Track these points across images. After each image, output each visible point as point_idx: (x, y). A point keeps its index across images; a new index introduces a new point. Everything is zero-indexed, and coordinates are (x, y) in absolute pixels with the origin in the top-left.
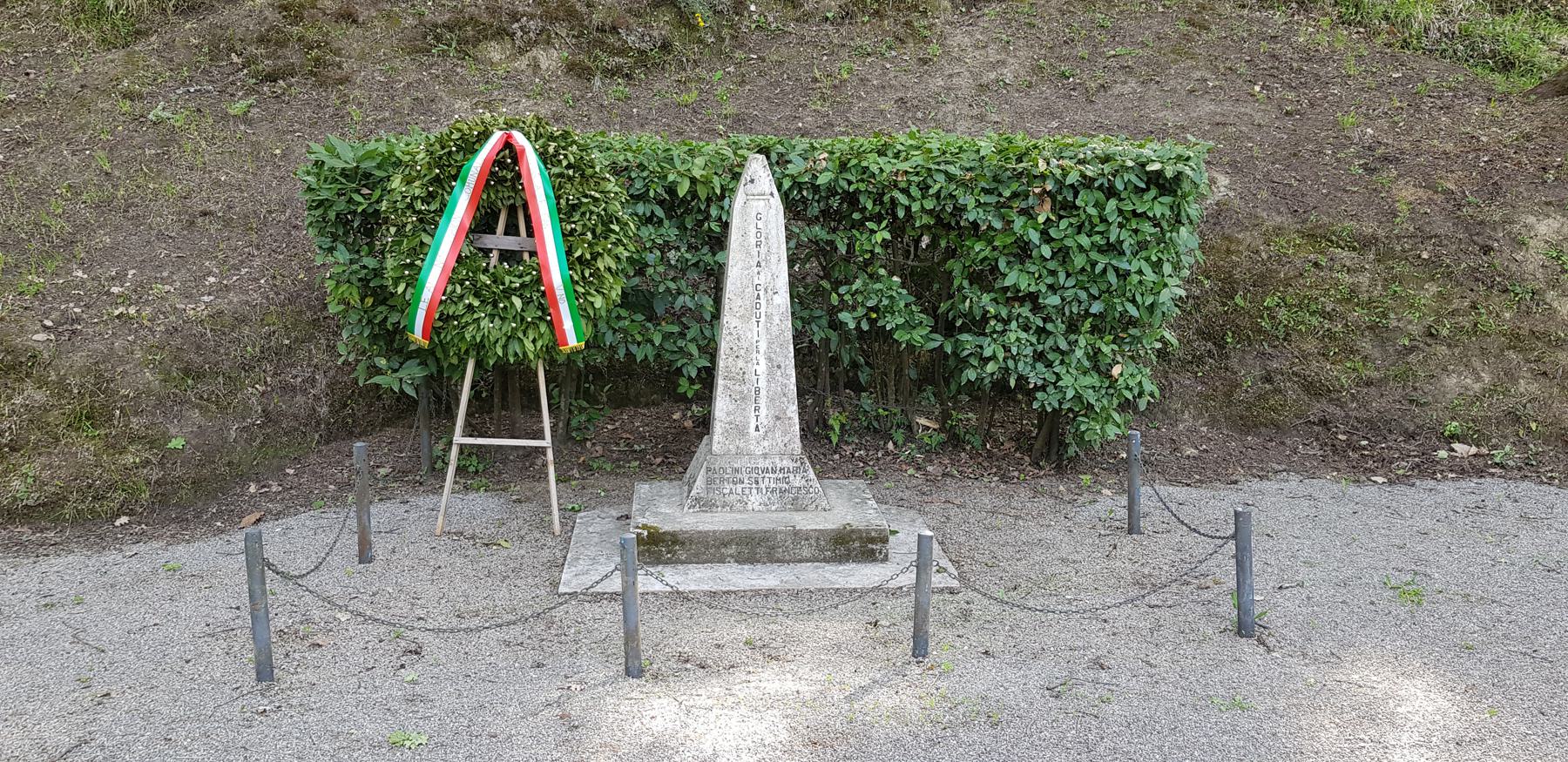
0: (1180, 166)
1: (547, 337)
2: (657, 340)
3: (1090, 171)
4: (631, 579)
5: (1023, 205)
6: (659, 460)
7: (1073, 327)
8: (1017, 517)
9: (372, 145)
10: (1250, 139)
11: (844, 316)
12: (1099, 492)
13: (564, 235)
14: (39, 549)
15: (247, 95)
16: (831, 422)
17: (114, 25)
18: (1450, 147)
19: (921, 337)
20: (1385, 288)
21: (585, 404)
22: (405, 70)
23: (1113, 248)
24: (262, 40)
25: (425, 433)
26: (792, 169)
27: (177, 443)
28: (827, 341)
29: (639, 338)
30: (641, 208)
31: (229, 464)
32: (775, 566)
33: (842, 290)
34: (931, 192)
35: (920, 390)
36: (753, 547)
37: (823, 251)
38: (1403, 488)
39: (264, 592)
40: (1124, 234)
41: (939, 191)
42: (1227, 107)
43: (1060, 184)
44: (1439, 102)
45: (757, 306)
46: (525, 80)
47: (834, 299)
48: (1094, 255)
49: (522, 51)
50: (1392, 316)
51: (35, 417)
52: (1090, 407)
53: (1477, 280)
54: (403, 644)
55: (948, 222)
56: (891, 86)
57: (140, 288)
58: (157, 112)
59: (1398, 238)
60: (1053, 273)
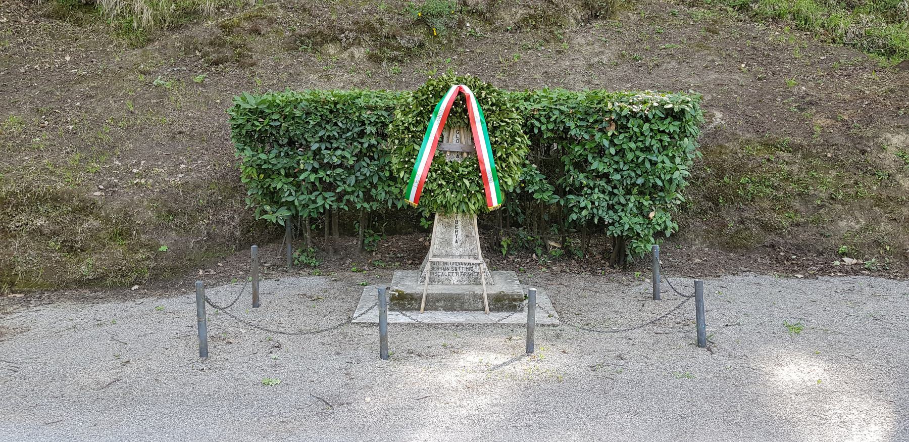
0: (683, 106)
3: (636, 109)
5: (600, 127)
7: (628, 192)
8: (596, 292)
9: (265, 96)
10: (736, 93)
12: (644, 281)
14: (95, 300)
15: (203, 72)
16: (502, 243)
17: (136, 36)
18: (847, 97)
19: (548, 196)
20: (807, 173)
21: (372, 232)
22: (285, 59)
23: (648, 149)
24: (211, 44)
25: (289, 246)
27: (163, 248)
31: (190, 260)
34: (552, 120)
36: (453, 303)
38: (812, 280)
39: (205, 313)
40: (654, 142)
42: (725, 75)
43: (619, 115)
44: (845, 73)
48: (638, 153)
49: (345, 49)
50: (811, 188)
51: (94, 234)
52: (638, 234)
53: (858, 168)
54: (272, 343)
55: (563, 135)
57: (147, 170)
58: (158, 81)
59: (815, 146)
60: (617, 163)
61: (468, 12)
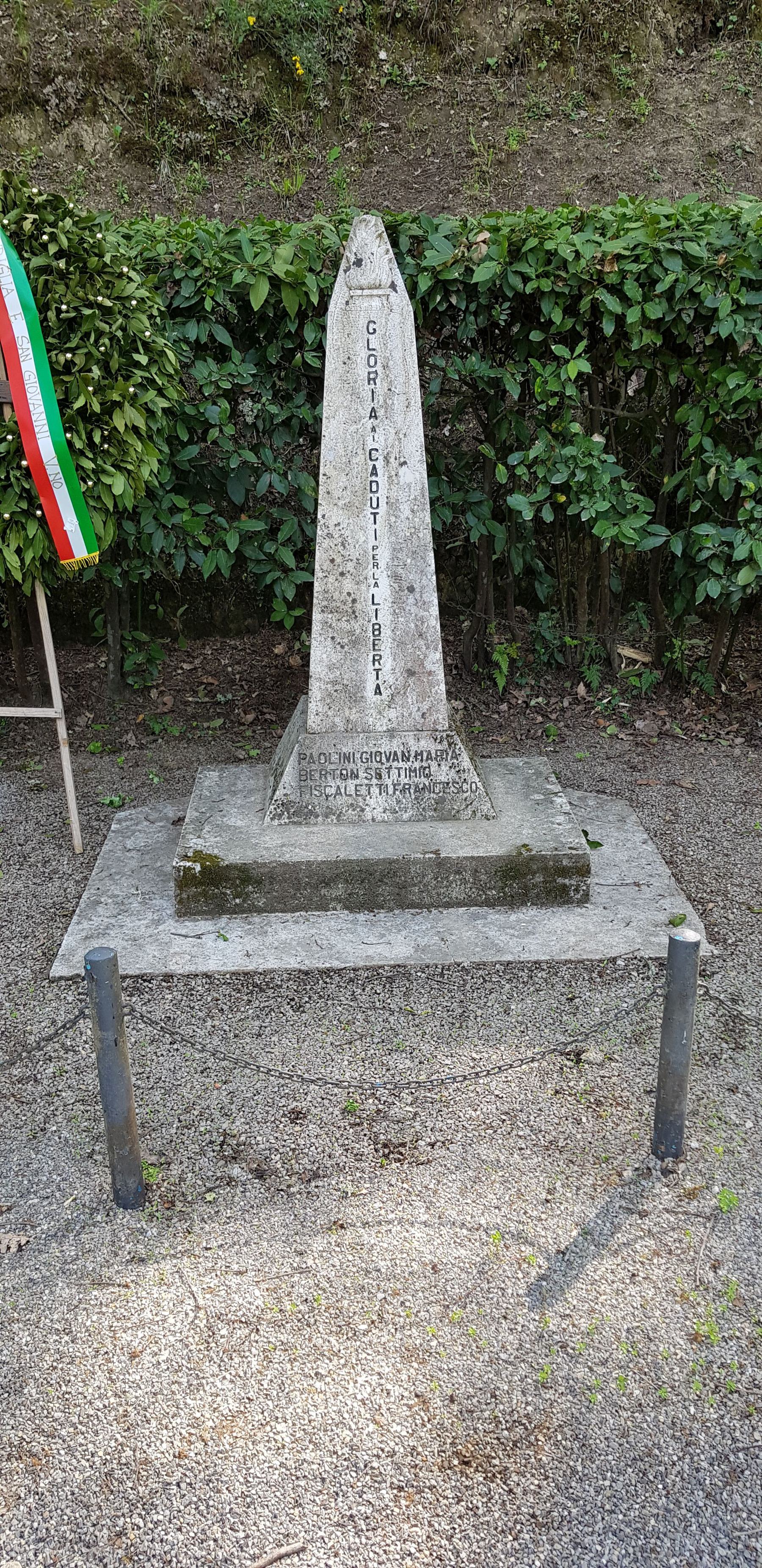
1: (41, 544)
2: (233, 544)
4: (110, 1036)
6: (250, 717)
11: (517, 501)
13: (55, 372)
16: (496, 657)
19: (636, 530)
26: (432, 258)
28: (489, 540)
29: (206, 541)
30: (193, 331)
32: (408, 913)
33: (514, 459)
34: (660, 288)
35: (627, 609)
36: (372, 887)
37: (484, 397)
41: (672, 288)
45: (372, 487)
46: (62, 167)
47: (501, 474)
49: (58, 127)
56: (580, 160)
61: (383, 19)
